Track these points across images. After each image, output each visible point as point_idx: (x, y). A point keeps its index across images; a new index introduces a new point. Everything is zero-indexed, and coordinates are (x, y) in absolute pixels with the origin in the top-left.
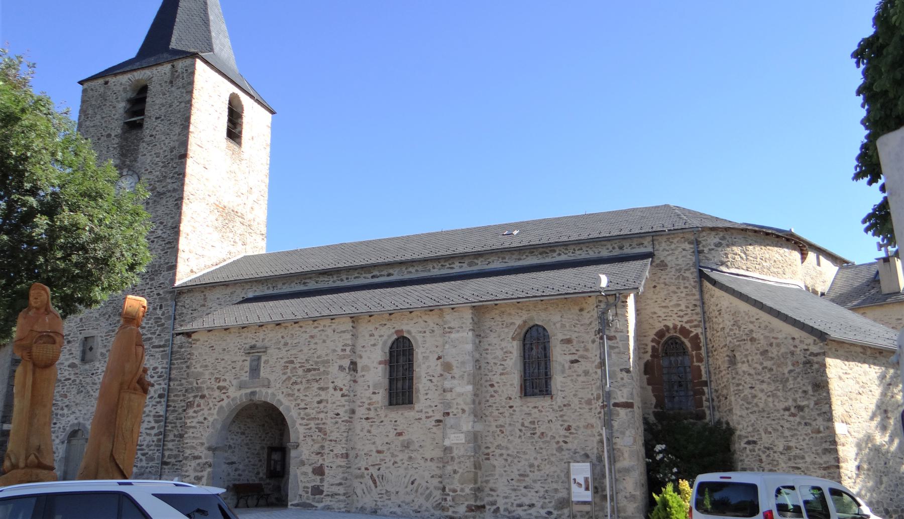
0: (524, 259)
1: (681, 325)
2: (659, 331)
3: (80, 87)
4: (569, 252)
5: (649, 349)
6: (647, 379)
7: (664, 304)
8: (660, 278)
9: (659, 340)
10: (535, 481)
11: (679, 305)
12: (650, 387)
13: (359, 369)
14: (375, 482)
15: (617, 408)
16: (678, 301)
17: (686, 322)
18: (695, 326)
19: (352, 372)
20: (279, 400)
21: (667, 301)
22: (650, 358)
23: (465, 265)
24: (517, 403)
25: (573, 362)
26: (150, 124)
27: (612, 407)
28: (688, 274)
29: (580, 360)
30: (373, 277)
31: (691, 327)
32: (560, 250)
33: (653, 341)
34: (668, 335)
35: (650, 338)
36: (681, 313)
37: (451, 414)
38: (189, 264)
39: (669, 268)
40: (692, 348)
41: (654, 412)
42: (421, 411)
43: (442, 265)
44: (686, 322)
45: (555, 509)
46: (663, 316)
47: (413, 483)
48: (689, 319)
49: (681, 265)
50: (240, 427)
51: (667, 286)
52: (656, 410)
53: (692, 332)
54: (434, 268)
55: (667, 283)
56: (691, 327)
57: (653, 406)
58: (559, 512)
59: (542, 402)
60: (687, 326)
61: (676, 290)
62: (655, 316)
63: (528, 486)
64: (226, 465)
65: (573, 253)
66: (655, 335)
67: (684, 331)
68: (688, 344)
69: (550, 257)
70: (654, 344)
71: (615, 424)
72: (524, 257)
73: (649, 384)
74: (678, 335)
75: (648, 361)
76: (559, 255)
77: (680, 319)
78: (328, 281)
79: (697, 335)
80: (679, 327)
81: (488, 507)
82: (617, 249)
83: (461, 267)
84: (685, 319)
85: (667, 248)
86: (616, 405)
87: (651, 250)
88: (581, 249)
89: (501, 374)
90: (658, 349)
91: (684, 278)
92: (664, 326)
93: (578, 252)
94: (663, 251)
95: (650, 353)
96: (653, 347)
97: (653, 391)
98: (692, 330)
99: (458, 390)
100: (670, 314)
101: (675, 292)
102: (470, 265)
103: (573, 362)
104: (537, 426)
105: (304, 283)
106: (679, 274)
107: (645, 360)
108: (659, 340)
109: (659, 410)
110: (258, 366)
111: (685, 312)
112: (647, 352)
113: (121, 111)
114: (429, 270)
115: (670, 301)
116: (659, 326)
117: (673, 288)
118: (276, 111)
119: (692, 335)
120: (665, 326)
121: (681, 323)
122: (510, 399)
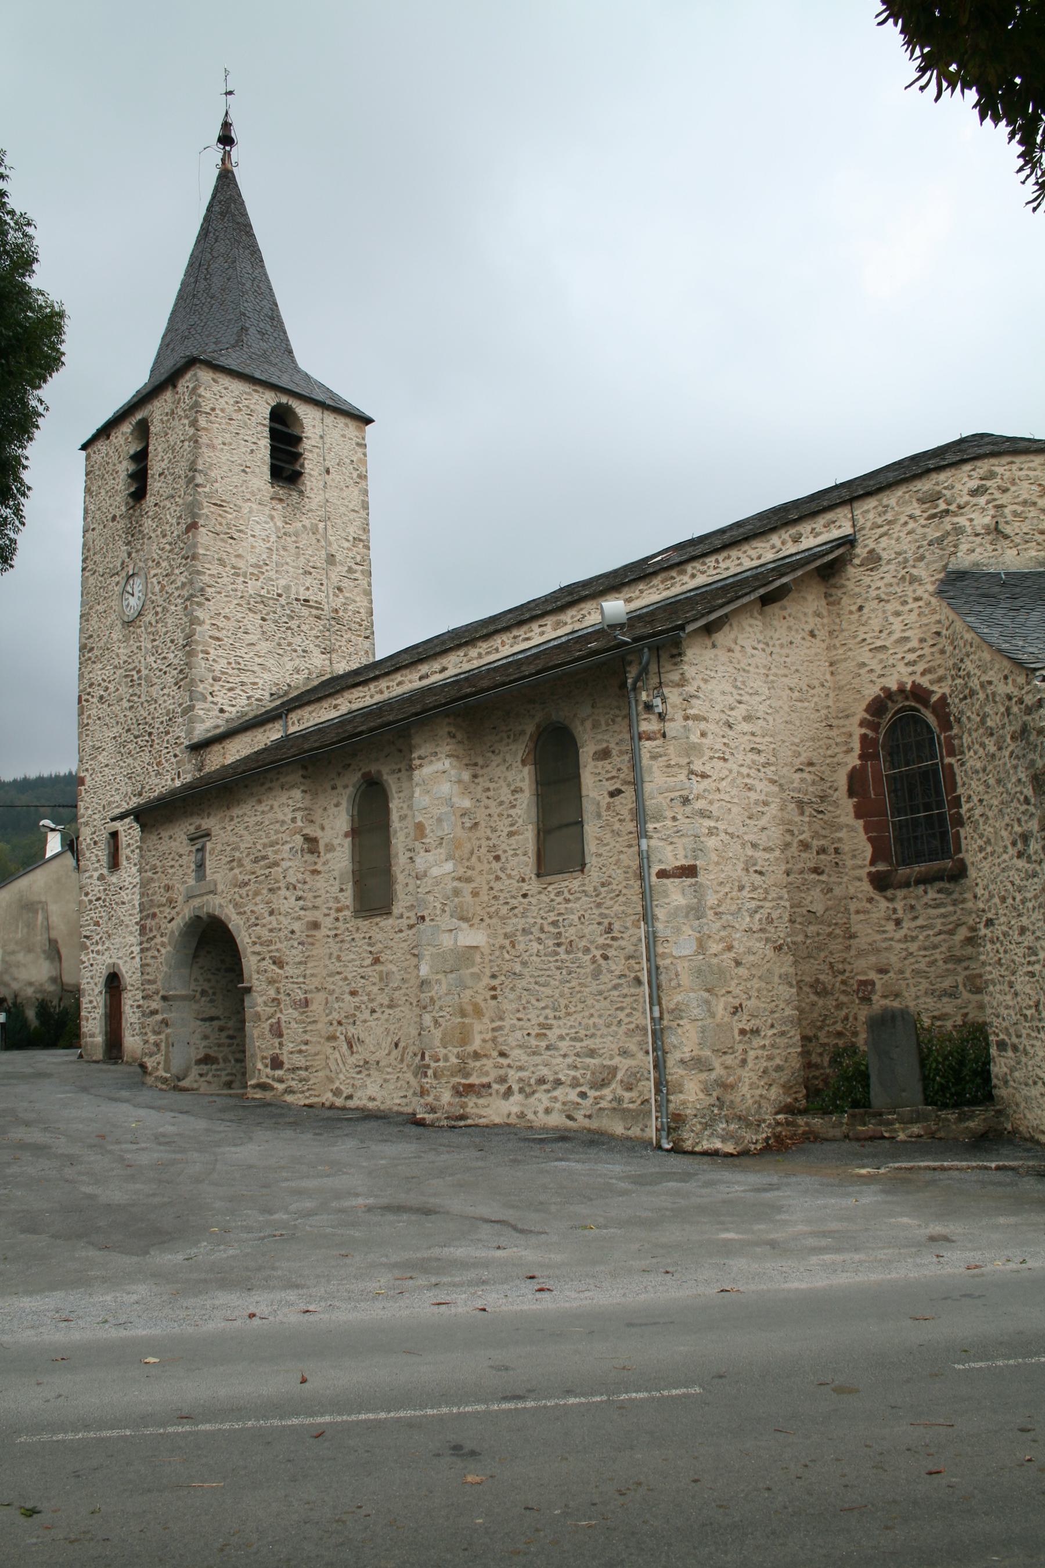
0: (638, 598)
1: (913, 682)
2: (873, 700)
3: (83, 453)
4: (709, 567)
5: (856, 745)
6: (854, 806)
7: (879, 643)
8: (869, 587)
9: (876, 720)
10: (561, 1038)
11: (906, 639)
12: (861, 823)
13: (322, 849)
14: (351, 1047)
15: (665, 881)
16: (903, 631)
17: (923, 674)
18: (940, 680)
19: (308, 857)
20: (227, 915)
21: (884, 635)
22: (858, 762)
23: (548, 629)
24: (533, 886)
25: (612, 794)
26: (155, 485)
27: (654, 879)
28: (921, 571)
29: (623, 788)
30: (421, 678)
31: (932, 682)
32: (694, 568)
33: (862, 724)
34: (893, 708)
35: (856, 720)
36: (911, 657)
37: (427, 919)
38: (215, 700)
39: (883, 562)
40: (939, 725)
41: (869, 874)
42: (401, 917)
43: (515, 637)
44: (923, 674)
45: (591, 1088)
46: (878, 669)
47: (397, 1045)
48: (926, 666)
49: (905, 552)
50: (223, 961)
51: (883, 603)
52: (873, 869)
53: (933, 692)
54: (503, 644)
55: (883, 596)
56: (932, 682)
57: (867, 862)
58: (598, 1093)
59: (573, 883)
60: (924, 682)
61: (900, 608)
62: (863, 671)
63: (551, 1045)
64: (199, 1023)
65: (715, 568)
66: (866, 710)
67: (919, 694)
68: (931, 719)
69: (678, 585)
70: (863, 731)
71: (660, 913)
72: (637, 593)
73: (858, 816)
74: (913, 704)
75: (854, 768)
76: (693, 576)
77: (910, 669)
78: (365, 696)
79: (943, 697)
80: (909, 687)
81: (495, 1086)
82: (790, 543)
83: (542, 633)
84: (920, 668)
85: (879, 521)
86: (662, 874)
87: (850, 531)
88: (729, 557)
89: (511, 834)
90: (876, 740)
91: (914, 580)
92: (881, 689)
93: (723, 565)
94: (872, 529)
95: (857, 751)
96: (864, 738)
97: (867, 829)
98: (935, 688)
99: (435, 871)
100: (891, 662)
101: (897, 614)
102: (558, 625)
103: (612, 794)
104: (562, 929)
105: (335, 707)
106: (903, 572)
107: (850, 767)
108: (876, 720)
109: (882, 867)
110: (203, 859)
111: (919, 653)
112: (851, 750)
113: (123, 475)
114: (497, 650)
115: (890, 633)
116: (872, 691)
117: (893, 606)
118: (369, 413)
119: (934, 698)
120: (884, 689)
121: (913, 678)
122: (523, 880)
